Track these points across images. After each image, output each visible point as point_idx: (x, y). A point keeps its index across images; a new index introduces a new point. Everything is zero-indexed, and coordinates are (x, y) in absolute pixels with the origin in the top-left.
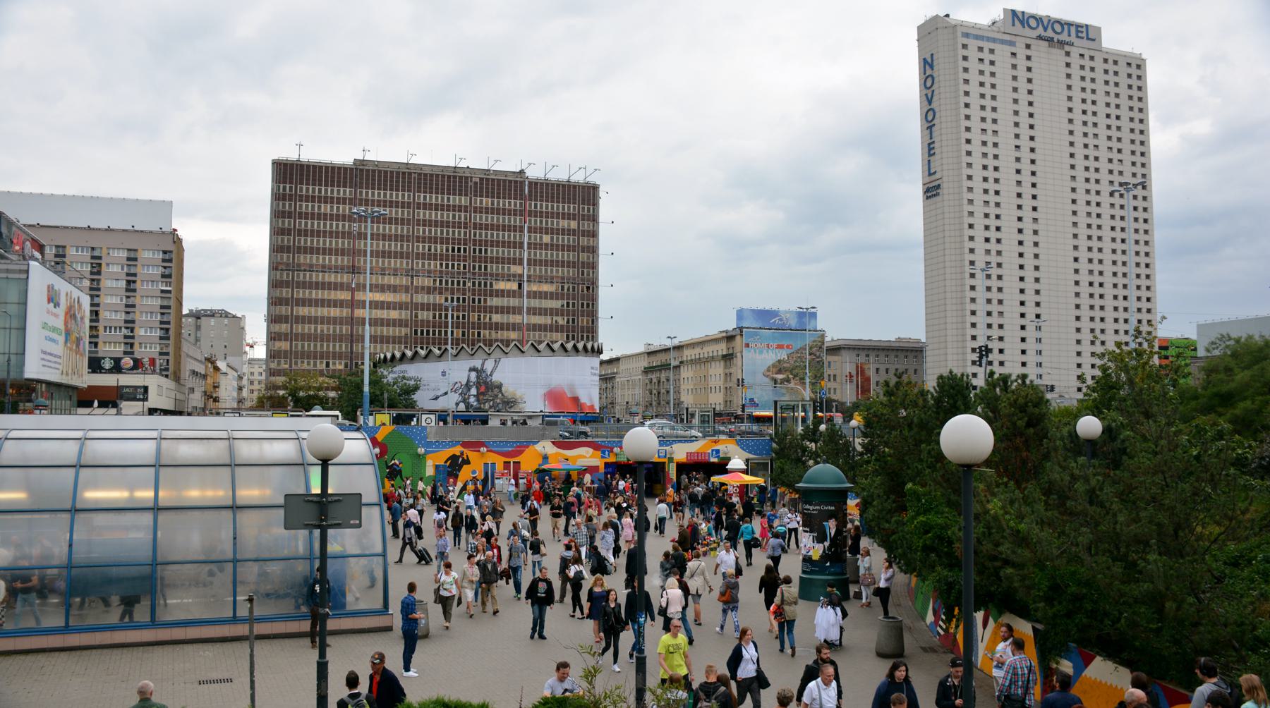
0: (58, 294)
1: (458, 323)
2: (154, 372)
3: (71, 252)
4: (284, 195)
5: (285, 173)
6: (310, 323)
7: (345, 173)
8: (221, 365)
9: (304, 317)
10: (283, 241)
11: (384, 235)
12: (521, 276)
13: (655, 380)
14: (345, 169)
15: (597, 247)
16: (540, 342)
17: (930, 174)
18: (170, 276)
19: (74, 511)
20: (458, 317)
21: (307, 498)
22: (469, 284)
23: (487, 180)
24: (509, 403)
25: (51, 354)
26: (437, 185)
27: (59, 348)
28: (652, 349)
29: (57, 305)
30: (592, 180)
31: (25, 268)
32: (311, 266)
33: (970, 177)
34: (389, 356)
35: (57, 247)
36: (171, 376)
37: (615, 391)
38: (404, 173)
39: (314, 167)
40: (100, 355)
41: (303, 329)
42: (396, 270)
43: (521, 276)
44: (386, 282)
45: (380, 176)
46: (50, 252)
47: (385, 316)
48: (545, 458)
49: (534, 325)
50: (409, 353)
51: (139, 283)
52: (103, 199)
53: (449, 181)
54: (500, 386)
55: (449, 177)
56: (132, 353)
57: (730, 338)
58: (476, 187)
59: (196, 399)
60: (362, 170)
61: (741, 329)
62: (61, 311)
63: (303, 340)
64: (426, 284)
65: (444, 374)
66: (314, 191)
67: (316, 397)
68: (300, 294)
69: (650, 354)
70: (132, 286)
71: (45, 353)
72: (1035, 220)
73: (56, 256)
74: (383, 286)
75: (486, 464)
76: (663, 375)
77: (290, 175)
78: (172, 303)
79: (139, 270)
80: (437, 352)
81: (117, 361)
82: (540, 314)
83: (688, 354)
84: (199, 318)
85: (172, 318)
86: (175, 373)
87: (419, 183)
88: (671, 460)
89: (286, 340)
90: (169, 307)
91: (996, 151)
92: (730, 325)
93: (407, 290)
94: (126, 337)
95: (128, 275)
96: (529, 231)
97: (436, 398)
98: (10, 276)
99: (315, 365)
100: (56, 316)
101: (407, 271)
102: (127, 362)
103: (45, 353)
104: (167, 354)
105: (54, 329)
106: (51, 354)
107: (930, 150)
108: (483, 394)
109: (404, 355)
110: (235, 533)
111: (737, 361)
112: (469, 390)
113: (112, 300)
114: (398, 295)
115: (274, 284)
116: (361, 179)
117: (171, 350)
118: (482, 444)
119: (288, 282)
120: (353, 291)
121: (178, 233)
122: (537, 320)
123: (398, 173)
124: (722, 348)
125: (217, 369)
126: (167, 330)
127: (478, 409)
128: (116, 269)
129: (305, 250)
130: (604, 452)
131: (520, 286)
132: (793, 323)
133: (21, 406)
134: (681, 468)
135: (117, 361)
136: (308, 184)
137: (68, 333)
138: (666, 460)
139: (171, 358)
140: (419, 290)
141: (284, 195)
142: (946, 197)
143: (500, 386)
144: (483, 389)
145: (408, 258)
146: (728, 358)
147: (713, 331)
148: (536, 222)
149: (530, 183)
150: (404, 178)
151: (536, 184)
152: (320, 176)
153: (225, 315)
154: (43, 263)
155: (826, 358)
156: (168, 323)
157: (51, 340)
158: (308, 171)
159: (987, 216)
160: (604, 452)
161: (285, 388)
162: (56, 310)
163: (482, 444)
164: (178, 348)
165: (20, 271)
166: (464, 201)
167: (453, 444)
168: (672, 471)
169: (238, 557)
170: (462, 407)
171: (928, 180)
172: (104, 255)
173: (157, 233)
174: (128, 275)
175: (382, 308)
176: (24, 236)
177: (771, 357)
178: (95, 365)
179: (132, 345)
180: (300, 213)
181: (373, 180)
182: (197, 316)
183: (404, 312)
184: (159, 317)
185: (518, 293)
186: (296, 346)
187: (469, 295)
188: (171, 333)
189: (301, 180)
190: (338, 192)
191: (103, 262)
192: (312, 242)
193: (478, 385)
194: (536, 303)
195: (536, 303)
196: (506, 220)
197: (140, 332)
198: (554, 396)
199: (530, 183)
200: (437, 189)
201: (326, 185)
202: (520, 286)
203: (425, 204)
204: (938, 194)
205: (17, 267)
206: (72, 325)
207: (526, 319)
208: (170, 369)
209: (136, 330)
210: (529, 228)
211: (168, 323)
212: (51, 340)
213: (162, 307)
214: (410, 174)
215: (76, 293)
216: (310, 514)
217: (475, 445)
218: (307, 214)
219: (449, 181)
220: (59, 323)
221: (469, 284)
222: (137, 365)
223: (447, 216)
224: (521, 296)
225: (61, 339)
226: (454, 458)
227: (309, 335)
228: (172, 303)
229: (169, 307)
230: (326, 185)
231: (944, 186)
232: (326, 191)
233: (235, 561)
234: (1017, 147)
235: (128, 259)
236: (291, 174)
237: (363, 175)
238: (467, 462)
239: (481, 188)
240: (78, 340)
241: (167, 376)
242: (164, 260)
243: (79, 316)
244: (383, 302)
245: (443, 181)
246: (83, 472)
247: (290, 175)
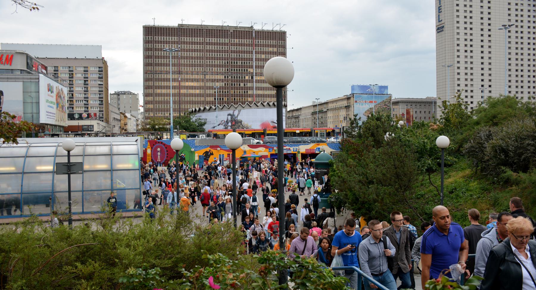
0: (52, 87)
1: (225, 95)
2: (96, 119)
3: (60, 69)
4: (149, 41)
5: (148, 31)
6: (161, 96)
7: (174, 30)
8: (127, 115)
9: (159, 94)
10: (149, 61)
11: (192, 57)
12: (252, 73)
14: (174, 29)
16: (264, 102)
17: (439, 21)
18: (102, 78)
19: (24, 173)
20: (225, 92)
21: (63, 164)
22: (230, 77)
23: (236, 31)
25: (51, 113)
26: (214, 34)
27: (54, 110)
28: (315, 104)
29: (52, 92)
30: (283, 29)
31: (37, 77)
32: (161, 71)
33: (458, 22)
34: (194, 109)
35: (55, 67)
36: (104, 121)
37: (300, 123)
38: (200, 29)
39: (161, 28)
40: (75, 112)
41: (159, 99)
42: (198, 72)
43: (252, 73)
44: (194, 77)
45: (189, 31)
46: (51, 69)
47: (194, 92)
48: (245, 152)
49: (259, 95)
50: (202, 108)
51: (89, 81)
53: (220, 32)
55: (220, 30)
56: (88, 111)
57: (348, 98)
58: (231, 34)
59: (116, 130)
60: (182, 29)
61: (353, 94)
62: (54, 95)
63: (159, 104)
64: (221, 78)
66: (161, 39)
67: (163, 128)
68: (157, 84)
69: (315, 106)
70: (87, 82)
71: (48, 112)
72: (490, 41)
73: (54, 71)
74: (192, 79)
75: (220, 155)
77: (150, 32)
78: (103, 89)
79: (89, 76)
80: (214, 107)
81: (80, 115)
82: (261, 90)
83: (330, 106)
84: (119, 95)
85: (104, 96)
86: (106, 119)
87: (207, 34)
88: (299, 152)
89: (152, 104)
90: (102, 91)
91: (471, 9)
92: (348, 92)
93: (203, 81)
94: (85, 104)
95: (84, 78)
96: (256, 53)
98: (32, 80)
99: (164, 114)
100: (52, 97)
101: (203, 72)
102: (85, 115)
103: (48, 112)
104: (102, 111)
105: (52, 102)
106: (51, 113)
107: (439, 10)
108: (234, 125)
109: (200, 109)
110: (83, 181)
111: (352, 109)
113: (78, 89)
114: (199, 83)
115: (146, 80)
116: (181, 33)
117: (104, 109)
118: (218, 147)
119: (151, 79)
120: (179, 82)
121: (105, 59)
122: (260, 92)
123: (197, 29)
124: (345, 103)
125: (126, 117)
126: (102, 101)
128: (79, 75)
129: (159, 65)
130: (270, 149)
131: (252, 77)
132: (377, 91)
133: (39, 135)
134: (304, 156)
135: (80, 115)
136: (158, 36)
137: (58, 104)
138: (296, 152)
139: (104, 113)
140: (208, 80)
141: (149, 41)
142: (446, 32)
143: (241, 122)
144: (234, 123)
145: (203, 67)
146: (347, 107)
147: (341, 95)
148: (258, 49)
149: (256, 32)
150: (200, 32)
151: (258, 32)
152: (164, 32)
153: (130, 93)
154: (46, 75)
155: (392, 107)
156: (102, 98)
157: (51, 107)
158: (158, 30)
159: (466, 40)
160: (270, 149)
161: (149, 124)
162: (52, 94)
163: (218, 147)
164: (107, 108)
165: (36, 79)
166: (227, 41)
167: (206, 147)
168: (299, 157)
169: (84, 189)
171: (438, 24)
172: (74, 69)
173: (96, 59)
174: (84, 78)
175: (192, 89)
176: (38, 64)
178: (71, 117)
179: (88, 108)
180: (156, 49)
181: (187, 33)
182: (118, 94)
183: (202, 90)
184: (98, 96)
185: (251, 81)
186: (156, 106)
187: (230, 82)
188: (104, 102)
189: (156, 34)
190: (172, 39)
191: (74, 73)
192: (161, 61)
193: (232, 121)
194: (259, 85)
195: (259, 85)
196: (245, 48)
197: (91, 102)
199: (256, 32)
200: (215, 36)
201: (166, 36)
202: (252, 77)
203: (209, 43)
204: (443, 31)
205: (34, 77)
206: (59, 100)
207: (255, 92)
208: (104, 118)
209: (89, 102)
210: (256, 52)
211: (102, 98)
212: (51, 107)
213: (99, 91)
214: (202, 30)
215: (61, 87)
216: (65, 169)
217: (215, 147)
218: (158, 49)
219: (220, 32)
220: (54, 100)
221: (230, 77)
222: (89, 116)
223: (215, 48)
224: (253, 82)
225: (55, 106)
226: (206, 153)
227: (162, 101)
228: (103, 89)
229: (102, 91)
230: (166, 36)
231: (446, 26)
232: (166, 38)
233: (83, 191)
234: (482, 7)
235: (84, 71)
236: (151, 32)
237: (182, 31)
238: (212, 154)
239: (234, 35)
240: (63, 107)
241: (103, 121)
242: (99, 71)
243: (62, 97)
244: (192, 86)
245: (217, 32)
246: (27, 159)
247: (150, 32)
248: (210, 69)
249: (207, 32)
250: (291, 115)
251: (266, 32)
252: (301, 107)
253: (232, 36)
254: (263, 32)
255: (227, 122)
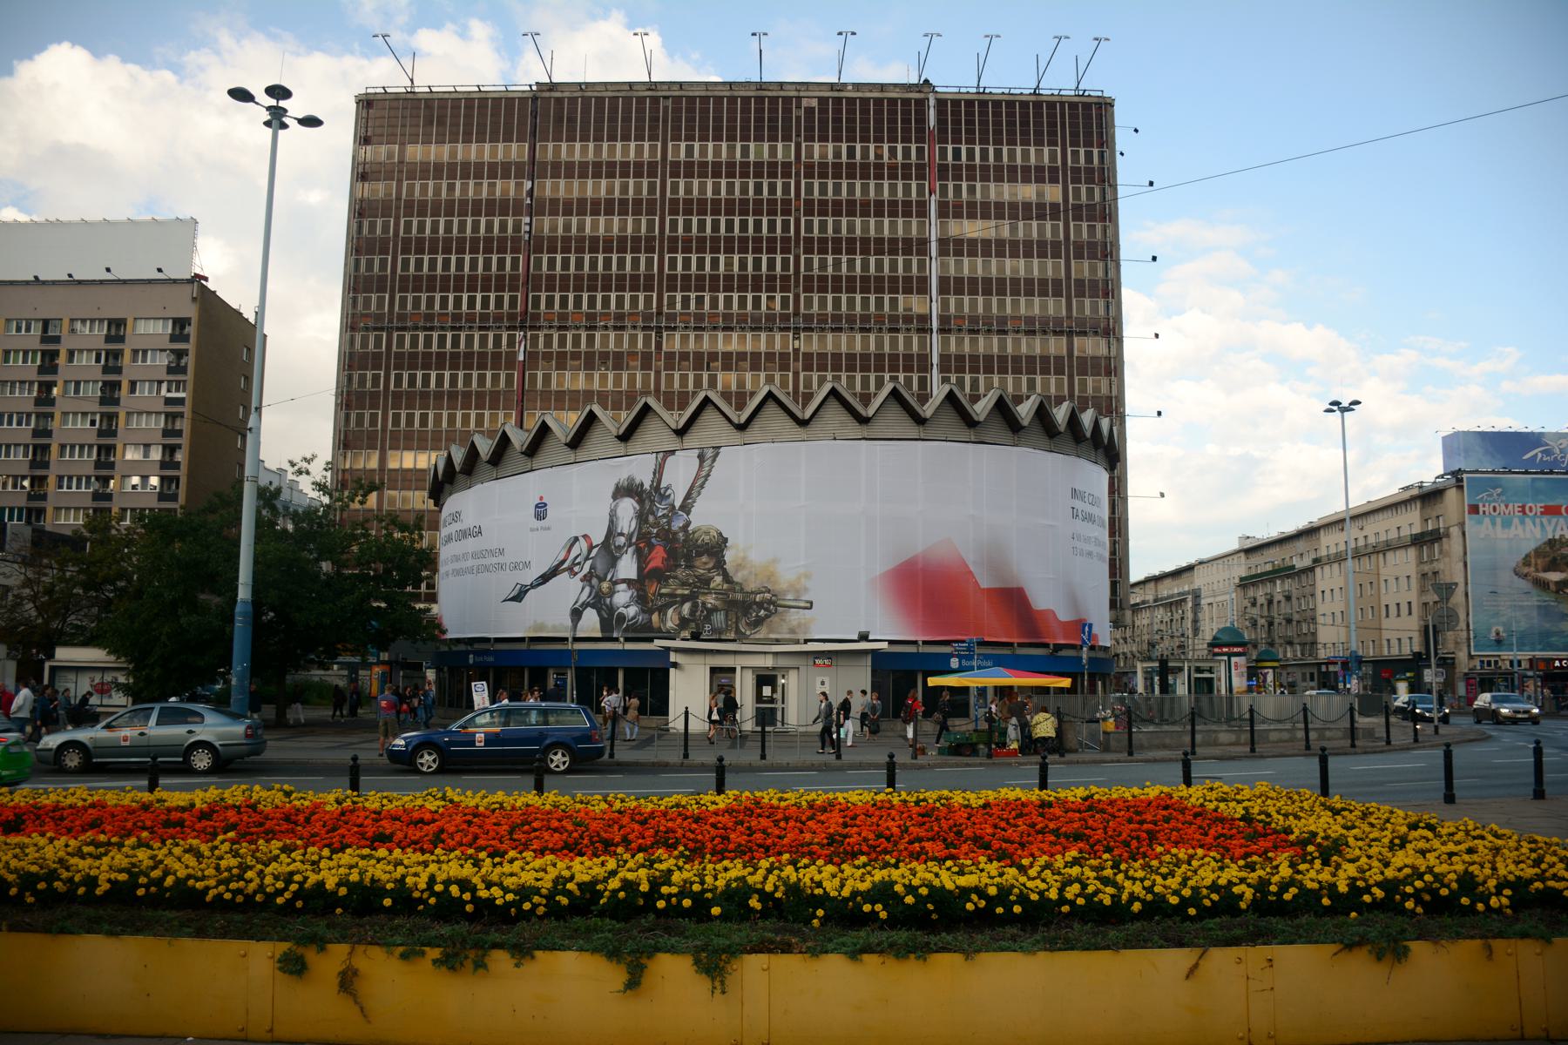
13: (1261, 600)
15: (1115, 244)
24: (752, 609)
30: (1095, 84)
52: (69, 224)
54: (717, 548)
57: (1428, 497)
65: (541, 511)
76: (1279, 588)
97: (518, 598)
112: (613, 562)
127: (643, 632)
143: (717, 548)
144: (658, 558)
149: (941, 103)
170: (591, 622)
177: (1530, 534)
198: (924, 585)
199: (941, 103)
248: (686, 301)
249: (677, 110)
250: (1150, 598)
251: (997, 104)
252: (1193, 561)
253: (810, 129)
254: (983, 104)
255: (609, 551)
